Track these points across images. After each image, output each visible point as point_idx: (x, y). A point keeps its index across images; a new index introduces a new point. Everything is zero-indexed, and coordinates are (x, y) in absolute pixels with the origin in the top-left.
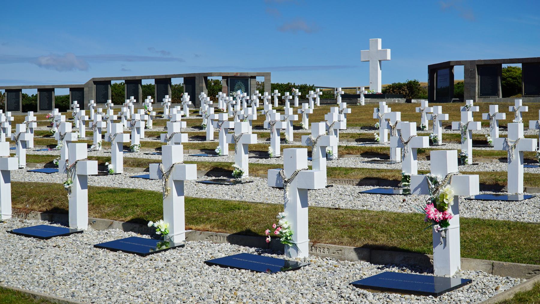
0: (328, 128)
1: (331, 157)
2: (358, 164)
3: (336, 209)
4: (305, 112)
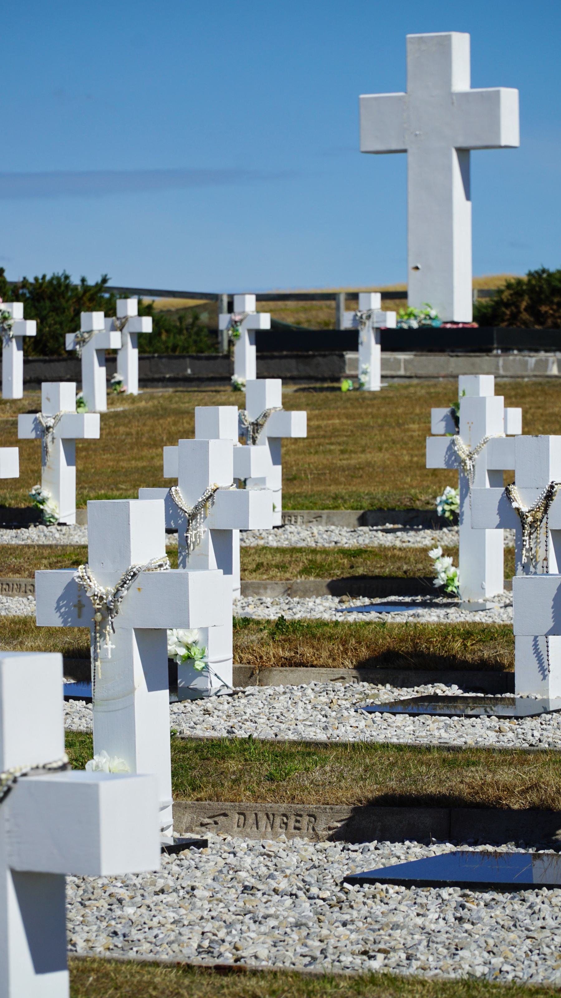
0: (178, 524)
1: (198, 683)
2: (340, 720)
3: (223, 970)
4: (60, 432)
